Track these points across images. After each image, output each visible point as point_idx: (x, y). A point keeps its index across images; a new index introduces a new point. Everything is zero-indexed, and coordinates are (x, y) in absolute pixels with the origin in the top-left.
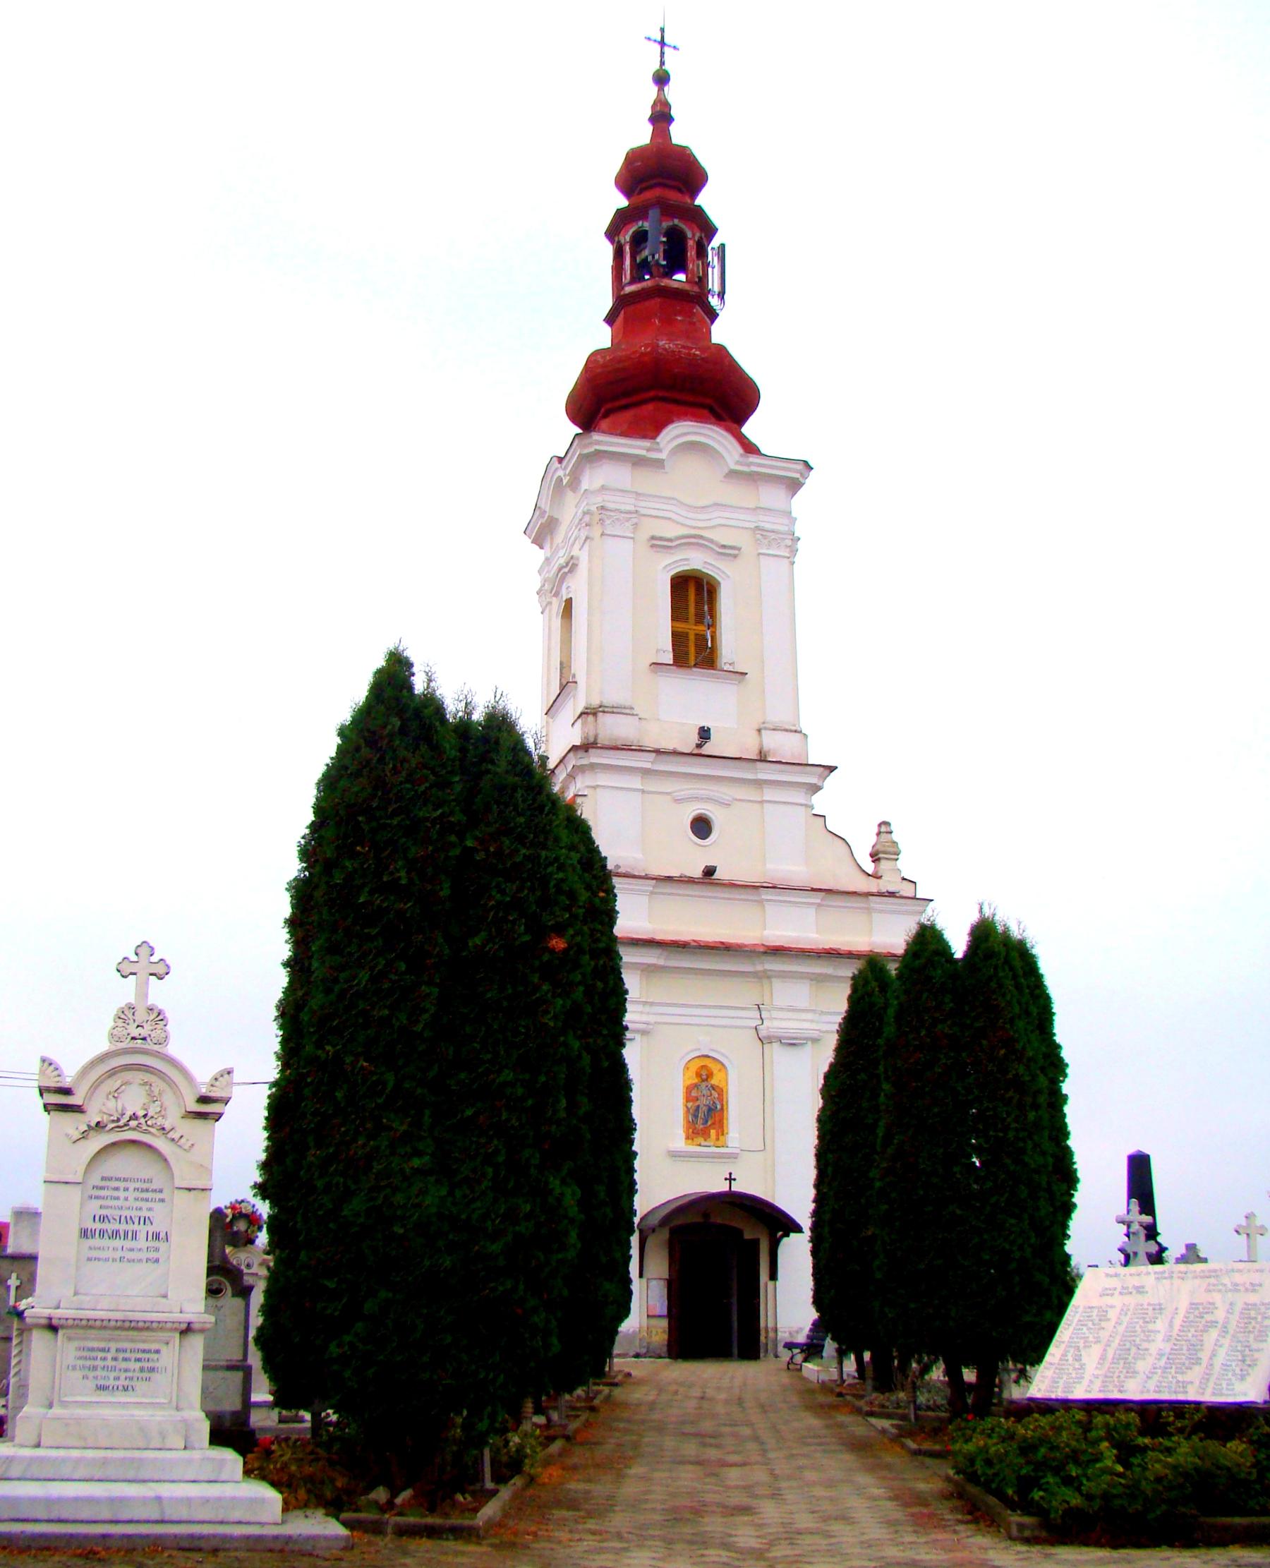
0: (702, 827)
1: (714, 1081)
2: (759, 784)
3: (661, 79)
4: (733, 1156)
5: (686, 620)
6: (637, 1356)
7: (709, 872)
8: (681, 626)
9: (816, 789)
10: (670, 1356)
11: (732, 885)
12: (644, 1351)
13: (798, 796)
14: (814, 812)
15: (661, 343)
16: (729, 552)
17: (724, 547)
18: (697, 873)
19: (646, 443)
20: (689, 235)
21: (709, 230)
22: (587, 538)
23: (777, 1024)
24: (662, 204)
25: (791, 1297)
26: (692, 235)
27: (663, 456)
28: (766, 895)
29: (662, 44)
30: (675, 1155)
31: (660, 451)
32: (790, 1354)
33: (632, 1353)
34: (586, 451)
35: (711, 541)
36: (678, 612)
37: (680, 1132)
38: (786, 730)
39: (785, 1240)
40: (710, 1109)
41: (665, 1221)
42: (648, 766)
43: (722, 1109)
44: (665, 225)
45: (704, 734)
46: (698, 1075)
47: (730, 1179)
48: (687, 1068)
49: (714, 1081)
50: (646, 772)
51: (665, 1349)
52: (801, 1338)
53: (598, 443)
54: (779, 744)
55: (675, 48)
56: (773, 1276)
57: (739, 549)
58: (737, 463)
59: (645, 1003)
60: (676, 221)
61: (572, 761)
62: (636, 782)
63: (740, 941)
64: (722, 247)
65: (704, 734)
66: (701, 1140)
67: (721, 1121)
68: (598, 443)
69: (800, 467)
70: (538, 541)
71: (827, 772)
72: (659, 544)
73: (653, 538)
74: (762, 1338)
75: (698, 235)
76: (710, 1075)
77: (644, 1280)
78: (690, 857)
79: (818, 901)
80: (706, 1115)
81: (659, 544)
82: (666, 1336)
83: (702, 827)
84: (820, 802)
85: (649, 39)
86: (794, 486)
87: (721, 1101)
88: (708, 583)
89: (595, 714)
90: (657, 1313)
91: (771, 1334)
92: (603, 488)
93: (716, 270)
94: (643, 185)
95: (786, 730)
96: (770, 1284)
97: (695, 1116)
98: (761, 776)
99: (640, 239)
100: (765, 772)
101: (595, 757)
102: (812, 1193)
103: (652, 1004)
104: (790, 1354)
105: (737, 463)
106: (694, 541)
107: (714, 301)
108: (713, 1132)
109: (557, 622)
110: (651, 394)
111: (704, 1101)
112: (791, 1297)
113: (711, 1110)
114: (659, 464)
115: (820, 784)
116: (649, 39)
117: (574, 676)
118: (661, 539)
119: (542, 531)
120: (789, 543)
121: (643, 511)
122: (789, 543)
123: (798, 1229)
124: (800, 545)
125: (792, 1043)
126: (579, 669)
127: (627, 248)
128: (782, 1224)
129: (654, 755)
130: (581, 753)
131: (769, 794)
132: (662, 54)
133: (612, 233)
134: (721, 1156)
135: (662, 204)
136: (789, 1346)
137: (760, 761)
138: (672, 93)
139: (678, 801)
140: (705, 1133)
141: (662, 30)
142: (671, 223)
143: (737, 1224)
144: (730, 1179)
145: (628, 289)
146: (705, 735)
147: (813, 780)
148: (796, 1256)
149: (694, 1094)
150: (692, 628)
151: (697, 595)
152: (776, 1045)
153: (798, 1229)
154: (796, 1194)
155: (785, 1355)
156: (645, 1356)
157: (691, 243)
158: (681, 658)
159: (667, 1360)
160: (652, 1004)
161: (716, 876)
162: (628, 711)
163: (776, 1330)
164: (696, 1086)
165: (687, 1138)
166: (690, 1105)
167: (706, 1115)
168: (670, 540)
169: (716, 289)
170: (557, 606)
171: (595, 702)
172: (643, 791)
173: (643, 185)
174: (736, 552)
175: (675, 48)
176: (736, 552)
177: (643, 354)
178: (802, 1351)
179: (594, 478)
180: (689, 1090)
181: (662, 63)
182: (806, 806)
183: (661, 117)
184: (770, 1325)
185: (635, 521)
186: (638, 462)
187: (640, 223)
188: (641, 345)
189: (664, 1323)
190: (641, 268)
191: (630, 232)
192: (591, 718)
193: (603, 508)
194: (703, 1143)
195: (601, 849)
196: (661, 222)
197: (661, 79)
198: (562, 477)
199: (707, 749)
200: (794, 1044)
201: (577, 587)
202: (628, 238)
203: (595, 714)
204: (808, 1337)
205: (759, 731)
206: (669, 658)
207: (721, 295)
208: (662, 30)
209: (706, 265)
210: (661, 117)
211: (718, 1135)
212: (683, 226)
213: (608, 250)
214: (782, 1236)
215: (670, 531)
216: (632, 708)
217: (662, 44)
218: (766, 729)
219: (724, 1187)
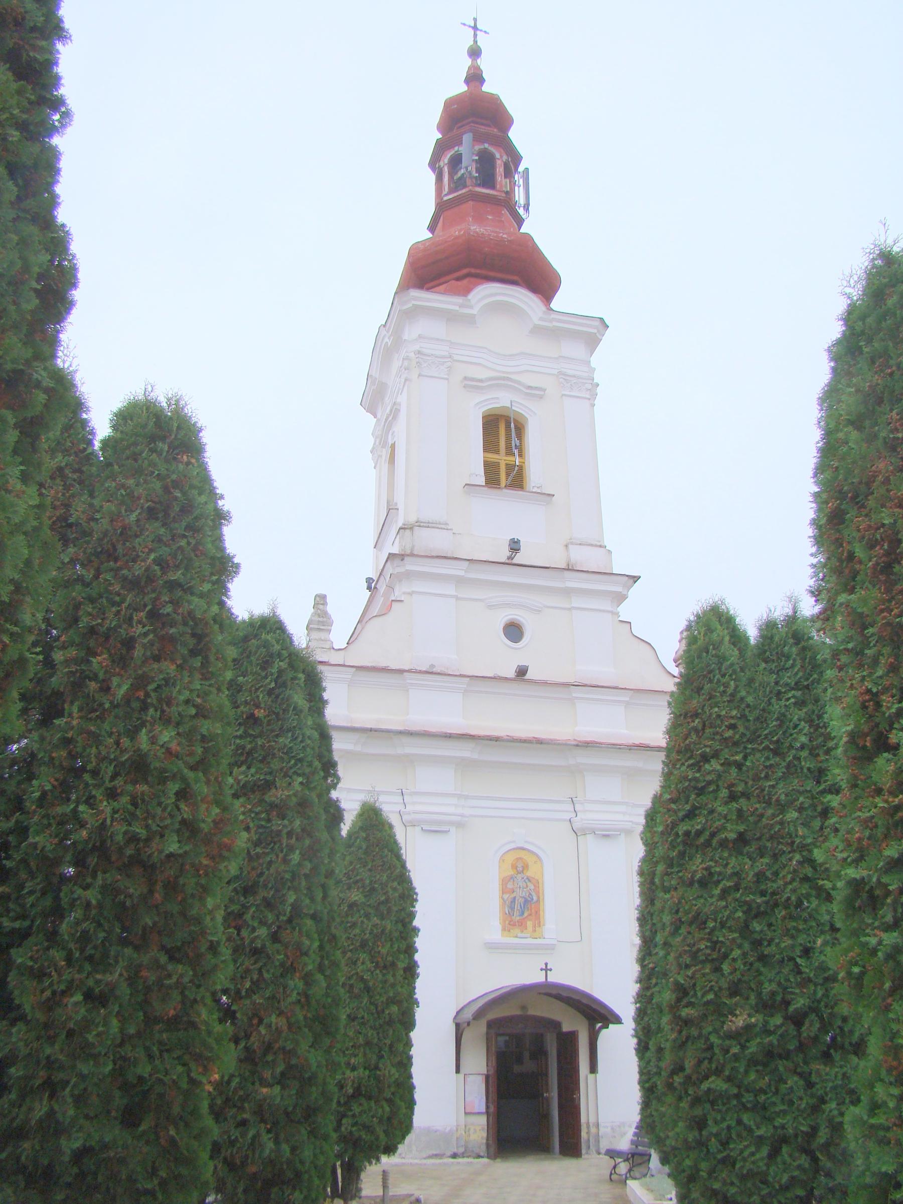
0: (514, 631)
1: (529, 873)
2: (568, 592)
3: (475, 53)
4: (551, 948)
5: (497, 452)
6: (454, 1156)
7: (522, 672)
8: (493, 457)
9: (621, 598)
10: (489, 1157)
11: (545, 683)
12: (461, 1150)
13: (607, 605)
14: (620, 619)
15: (472, 228)
16: (536, 393)
17: (530, 387)
18: (511, 674)
19: (459, 300)
20: (498, 156)
21: (516, 158)
22: (406, 380)
23: (590, 816)
24: (476, 141)
25: (614, 1091)
26: (500, 158)
27: (474, 311)
28: (577, 693)
29: (475, 28)
30: (492, 947)
31: (471, 307)
32: (612, 1162)
33: (449, 1153)
34: (405, 307)
35: (519, 383)
36: (490, 445)
37: (496, 923)
38: (592, 545)
39: (604, 1031)
40: (526, 901)
41: (478, 1015)
42: (462, 573)
43: (538, 901)
44: (477, 148)
45: (515, 546)
46: (514, 867)
47: (546, 969)
48: (502, 860)
49: (529, 873)
50: (460, 581)
51: (484, 1147)
52: (624, 1144)
53: (416, 299)
54: (583, 557)
55: (485, 32)
56: (593, 1069)
57: (544, 390)
58: (541, 319)
59: (460, 796)
60: (486, 145)
61: (390, 570)
62: (450, 590)
63: (552, 737)
64: (527, 169)
65: (515, 546)
66: (517, 931)
67: (537, 913)
68: (416, 299)
69: (597, 323)
70: (371, 409)
71: (632, 581)
72: (471, 385)
73: (465, 378)
74: (584, 1134)
75: (505, 158)
76: (526, 867)
77: (461, 1076)
78: (504, 659)
79: (627, 699)
80: (522, 907)
81: (471, 385)
82: (485, 1135)
83: (514, 631)
84: (625, 611)
85: (464, 25)
86: (592, 342)
87: (538, 893)
88: (516, 421)
89: (411, 529)
90: (476, 1110)
91: (593, 1130)
92: (420, 337)
93: (521, 188)
94: (460, 125)
95: (592, 545)
96: (591, 1076)
97: (512, 908)
98: (569, 584)
99: (456, 161)
100: (572, 581)
101: (410, 565)
102: (634, 970)
103: (467, 797)
104: (612, 1162)
105: (541, 319)
106: (502, 382)
107: (521, 211)
108: (529, 924)
109: (385, 467)
110: (465, 271)
111: (520, 894)
112: (614, 1091)
113: (527, 902)
114: (470, 320)
115: (625, 593)
116: (464, 25)
117: (396, 504)
118: (472, 379)
119: (374, 398)
120: (590, 387)
121: (456, 357)
122: (590, 387)
123: (618, 1020)
124: (599, 390)
125: (606, 835)
126: (400, 500)
127: (446, 169)
128: (598, 1015)
129: (467, 563)
130: (397, 561)
131: (577, 602)
132: (475, 36)
133: (434, 164)
134: (537, 947)
135: (476, 141)
136: (612, 1154)
137: (568, 569)
138: (482, 63)
139: (490, 607)
140: (522, 925)
141: (475, 20)
142: (482, 147)
143: (556, 1017)
144: (546, 969)
145: (445, 198)
146: (515, 546)
147: (619, 589)
148: (618, 1047)
149: (510, 886)
150: (502, 459)
151: (506, 430)
152: (590, 837)
153: (618, 1020)
154: (616, 982)
155: (606, 1162)
156: (463, 1155)
157: (499, 162)
158: (492, 477)
159: (486, 1160)
160: (467, 797)
161: (528, 676)
162: (443, 526)
163: (597, 1125)
164: (511, 878)
165: (504, 929)
166: (506, 896)
167: (522, 907)
168: (481, 381)
169: (522, 202)
170: (385, 453)
171: (412, 519)
172: (457, 598)
173: (460, 125)
174: (542, 393)
175: (485, 32)
176: (542, 393)
177: (457, 238)
178: (627, 1160)
179: (412, 332)
180: (504, 882)
181: (475, 42)
182: (612, 612)
183: (475, 77)
184: (592, 1120)
185: (449, 364)
186: (451, 318)
187: (456, 149)
188: (456, 231)
189: (483, 1120)
190: (458, 184)
191: (448, 156)
192: (408, 532)
193: (419, 352)
194: (520, 935)
195: (638, 1111)
196: (474, 146)
197: (475, 53)
198: (387, 347)
199: (518, 559)
200: (608, 836)
201: (400, 432)
202: (446, 161)
203: (411, 529)
204: (632, 1142)
205: (566, 546)
206: (482, 480)
207: (526, 208)
208: (475, 20)
209: (513, 184)
210: (475, 77)
211: (534, 926)
212: (492, 149)
213: (432, 177)
214: (601, 1028)
215: (483, 374)
216: (446, 524)
217: (475, 28)
218: (572, 543)
219: (539, 978)
